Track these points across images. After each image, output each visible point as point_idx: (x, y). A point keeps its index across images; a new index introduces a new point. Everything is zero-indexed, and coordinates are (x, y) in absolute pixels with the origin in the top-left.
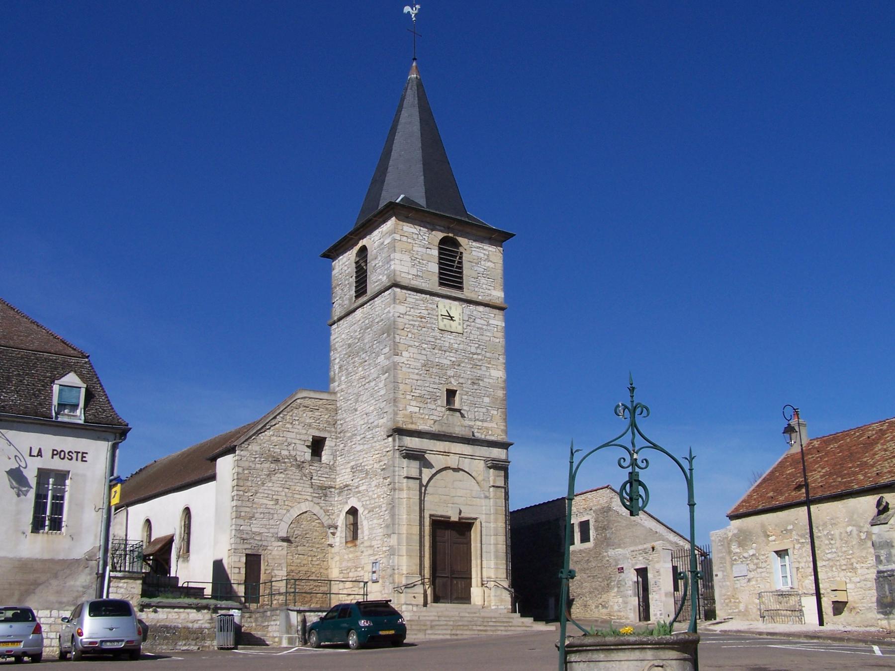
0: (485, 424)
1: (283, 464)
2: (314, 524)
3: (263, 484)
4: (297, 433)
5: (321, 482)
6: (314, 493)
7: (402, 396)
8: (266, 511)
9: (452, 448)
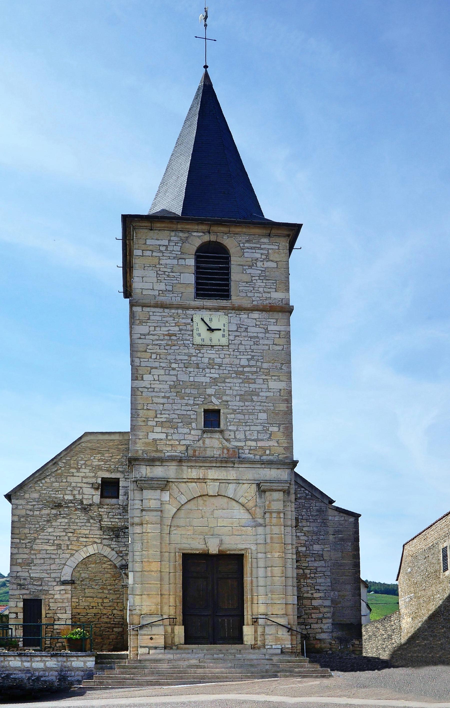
0: (260, 444)
1: (65, 509)
2: (104, 566)
3: (43, 530)
4: (83, 477)
5: (113, 523)
6: (103, 534)
7: (143, 424)
8: (48, 556)
9: (209, 473)
